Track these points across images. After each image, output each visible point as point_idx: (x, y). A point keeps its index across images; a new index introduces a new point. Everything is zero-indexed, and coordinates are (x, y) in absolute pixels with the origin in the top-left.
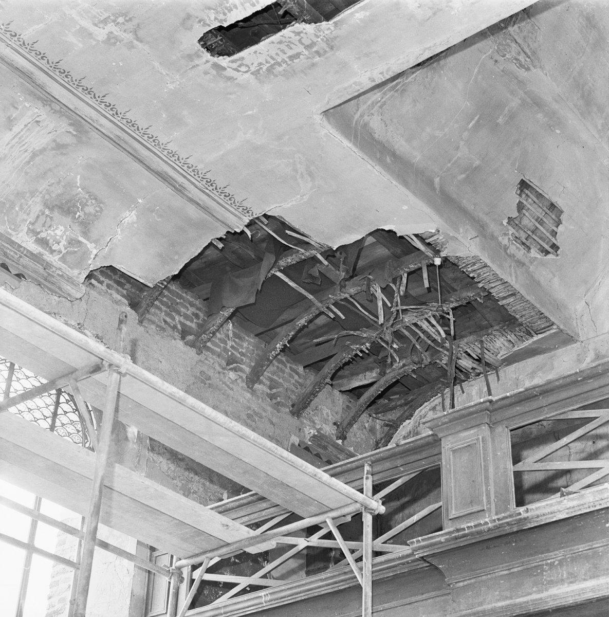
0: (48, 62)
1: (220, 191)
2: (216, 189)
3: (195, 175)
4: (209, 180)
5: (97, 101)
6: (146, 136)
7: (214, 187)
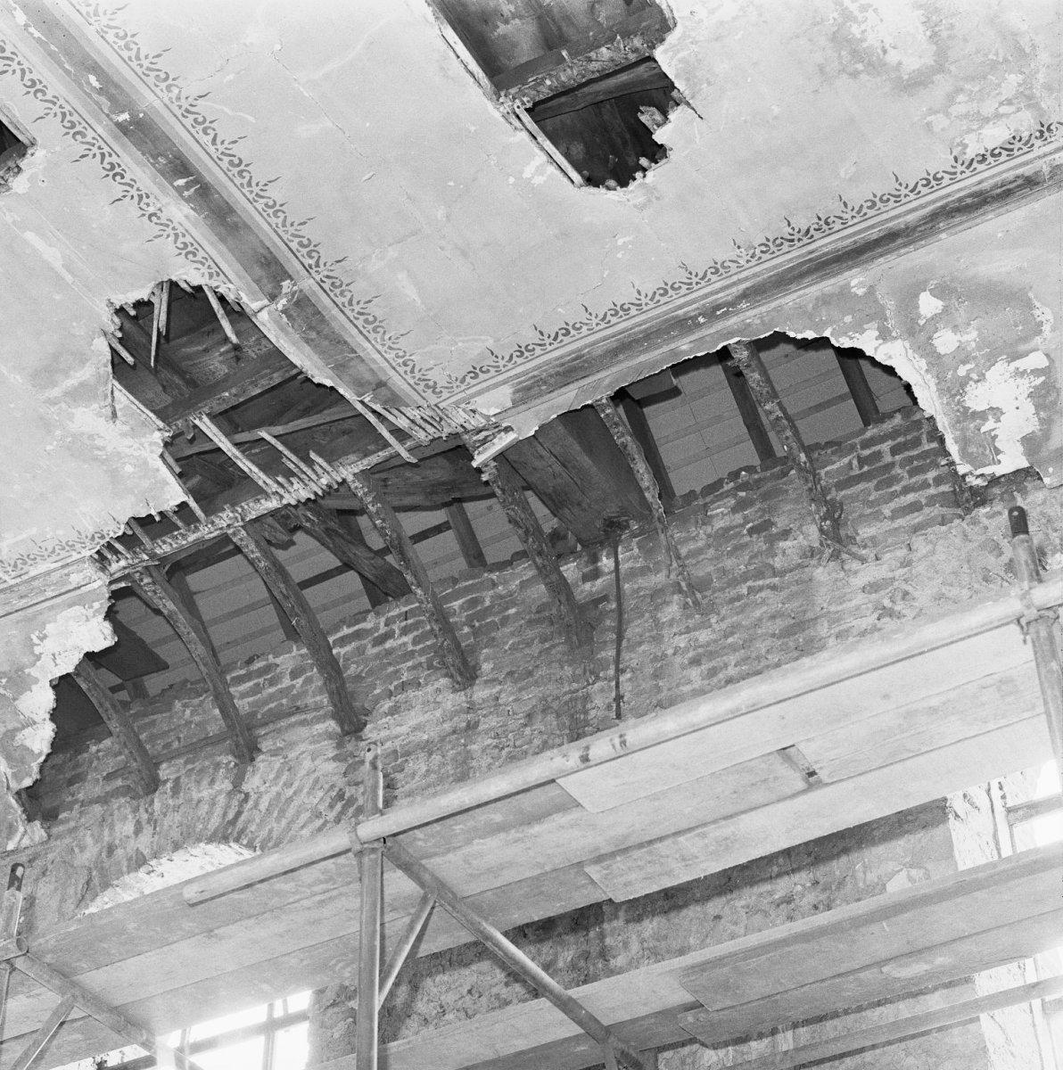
0: (214, 141)
1: (169, 230)
2: (64, 115)
3: (130, 58)
4: (190, 256)
5: (19, 63)
6: (89, 139)
7: (181, 239)
